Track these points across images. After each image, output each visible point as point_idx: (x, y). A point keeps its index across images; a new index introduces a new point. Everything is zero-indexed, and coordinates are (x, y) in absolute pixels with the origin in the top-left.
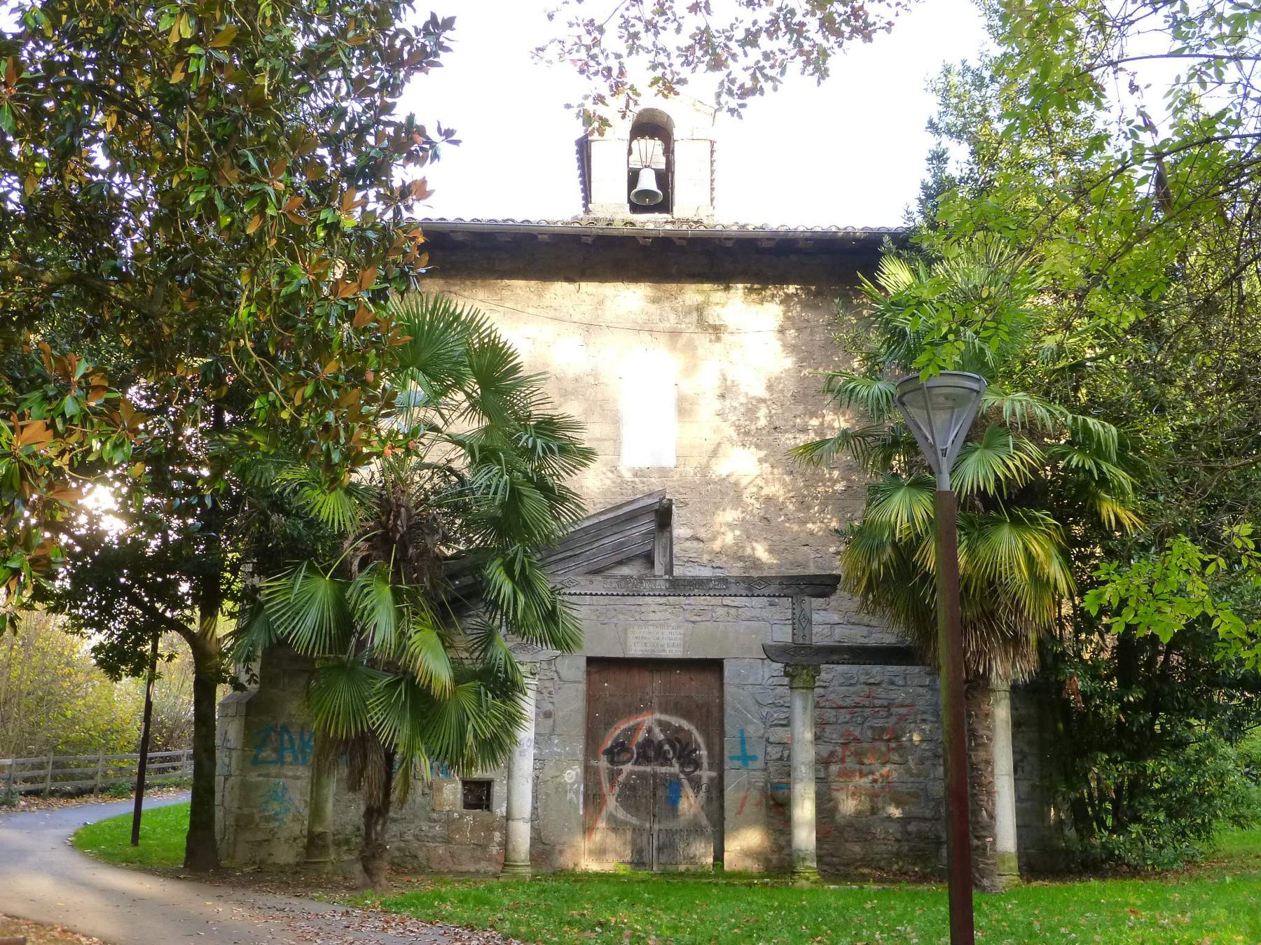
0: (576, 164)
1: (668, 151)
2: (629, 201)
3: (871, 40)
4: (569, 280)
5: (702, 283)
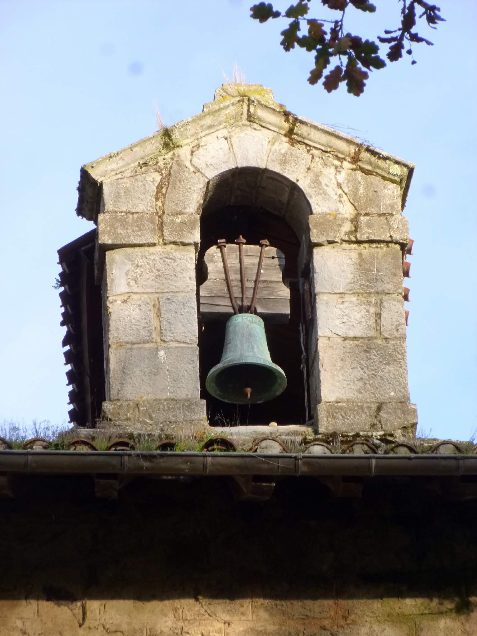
0: (57, 310)
1: (298, 273)
2: (204, 394)
3: (287, 49)
4: (58, 594)
5: (400, 595)
